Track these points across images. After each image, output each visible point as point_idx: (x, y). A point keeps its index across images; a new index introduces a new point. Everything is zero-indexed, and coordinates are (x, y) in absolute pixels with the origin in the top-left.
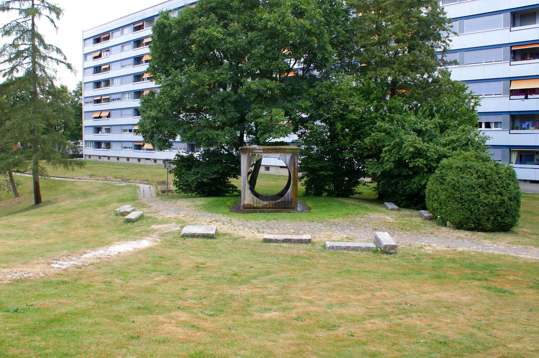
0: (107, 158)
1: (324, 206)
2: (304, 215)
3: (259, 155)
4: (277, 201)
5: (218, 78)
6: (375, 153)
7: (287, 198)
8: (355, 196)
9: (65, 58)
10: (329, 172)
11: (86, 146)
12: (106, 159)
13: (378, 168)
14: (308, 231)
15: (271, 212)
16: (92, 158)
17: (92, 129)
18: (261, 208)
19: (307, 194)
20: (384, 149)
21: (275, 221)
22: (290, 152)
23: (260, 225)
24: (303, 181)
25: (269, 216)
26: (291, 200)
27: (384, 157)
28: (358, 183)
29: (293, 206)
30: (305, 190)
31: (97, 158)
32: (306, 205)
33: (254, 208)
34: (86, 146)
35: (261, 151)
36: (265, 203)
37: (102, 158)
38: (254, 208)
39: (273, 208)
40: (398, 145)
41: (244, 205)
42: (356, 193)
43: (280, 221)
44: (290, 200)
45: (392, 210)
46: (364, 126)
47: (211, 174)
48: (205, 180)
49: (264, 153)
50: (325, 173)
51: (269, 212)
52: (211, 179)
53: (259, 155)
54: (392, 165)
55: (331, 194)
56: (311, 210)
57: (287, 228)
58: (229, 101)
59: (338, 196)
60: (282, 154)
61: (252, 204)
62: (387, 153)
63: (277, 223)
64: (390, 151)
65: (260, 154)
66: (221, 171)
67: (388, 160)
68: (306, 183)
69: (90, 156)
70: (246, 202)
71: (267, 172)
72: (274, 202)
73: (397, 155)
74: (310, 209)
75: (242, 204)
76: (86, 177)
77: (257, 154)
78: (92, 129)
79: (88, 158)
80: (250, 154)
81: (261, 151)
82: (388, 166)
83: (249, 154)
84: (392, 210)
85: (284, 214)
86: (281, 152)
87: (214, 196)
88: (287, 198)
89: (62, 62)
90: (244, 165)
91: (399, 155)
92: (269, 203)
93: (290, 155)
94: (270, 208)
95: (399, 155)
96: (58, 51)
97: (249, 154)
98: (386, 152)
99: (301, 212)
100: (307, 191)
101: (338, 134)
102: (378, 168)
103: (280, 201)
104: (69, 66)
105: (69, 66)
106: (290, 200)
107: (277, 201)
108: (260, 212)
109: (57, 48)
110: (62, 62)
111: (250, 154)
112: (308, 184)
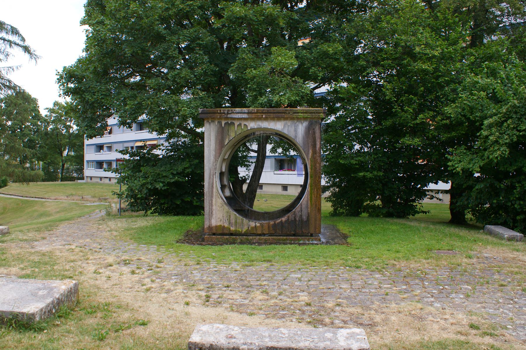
0: (108, 179)
1: (372, 232)
2: (335, 250)
3: (240, 125)
4: (279, 221)
5: (181, 6)
6: (467, 132)
7: (298, 214)
8: (417, 216)
9: (23, 40)
10: (375, 173)
11: (88, 167)
12: (107, 181)
13: (472, 160)
14: (347, 298)
15: (266, 243)
16: (94, 180)
17: (94, 147)
18: (246, 234)
19: (335, 214)
20: (486, 122)
21: (266, 265)
22: (305, 119)
23: (223, 276)
24: (327, 194)
25: (255, 252)
26: (308, 217)
27: (487, 137)
28: (422, 194)
29: (312, 231)
30: (332, 209)
31: (99, 180)
32: (338, 231)
33: (232, 234)
34: (88, 167)
35: (245, 116)
36: (252, 224)
37: (103, 180)
38: (232, 234)
39: (271, 235)
40: (516, 113)
41: (210, 228)
42: (418, 213)
43: (277, 266)
44: (305, 218)
45: (510, 239)
46: (442, 87)
47: (171, 176)
48: (159, 186)
49: (252, 119)
50: (369, 175)
51: (260, 244)
52: (169, 184)
53: (240, 125)
54: (505, 151)
55: (375, 213)
56: (349, 240)
57: (292, 286)
58: (199, 45)
59: (389, 215)
60: (289, 123)
61: (226, 225)
62: (494, 130)
63: (267, 270)
64: (499, 124)
65: (243, 123)
66: (190, 170)
67: (496, 142)
68: (334, 195)
69: (91, 178)
70: (214, 222)
71: (285, 193)
72: (272, 223)
73: (515, 132)
74: (345, 237)
75: (206, 226)
76: (63, 197)
77: (237, 123)
78: (93, 148)
79: (89, 180)
80: (223, 123)
81: (245, 116)
82: (499, 153)
83: (220, 123)
84: (510, 239)
85: (289, 249)
86: (286, 119)
87: (177, 214)
88: (298, 214)
89: (18, 45)
90: (209, 145)
91: (520, 131)
92: (262, 226)
93: (306, 124)
94: (264, 235)
95: (520, 131)
96: (15, 31)
97: (220, 123)
98: (490, 126)
99: (327, 243)
100: (335, 210)
101: (389, 102)
102: (472, 160)
103: (284, 219)
104: (26, 49)
105: (26, 49)
106: (305, 218)
107: (279, 221)
108: (242, 243)
109: (12, 27)
110: (18, 45)
111: (223, 123)
112: (336, 199)
